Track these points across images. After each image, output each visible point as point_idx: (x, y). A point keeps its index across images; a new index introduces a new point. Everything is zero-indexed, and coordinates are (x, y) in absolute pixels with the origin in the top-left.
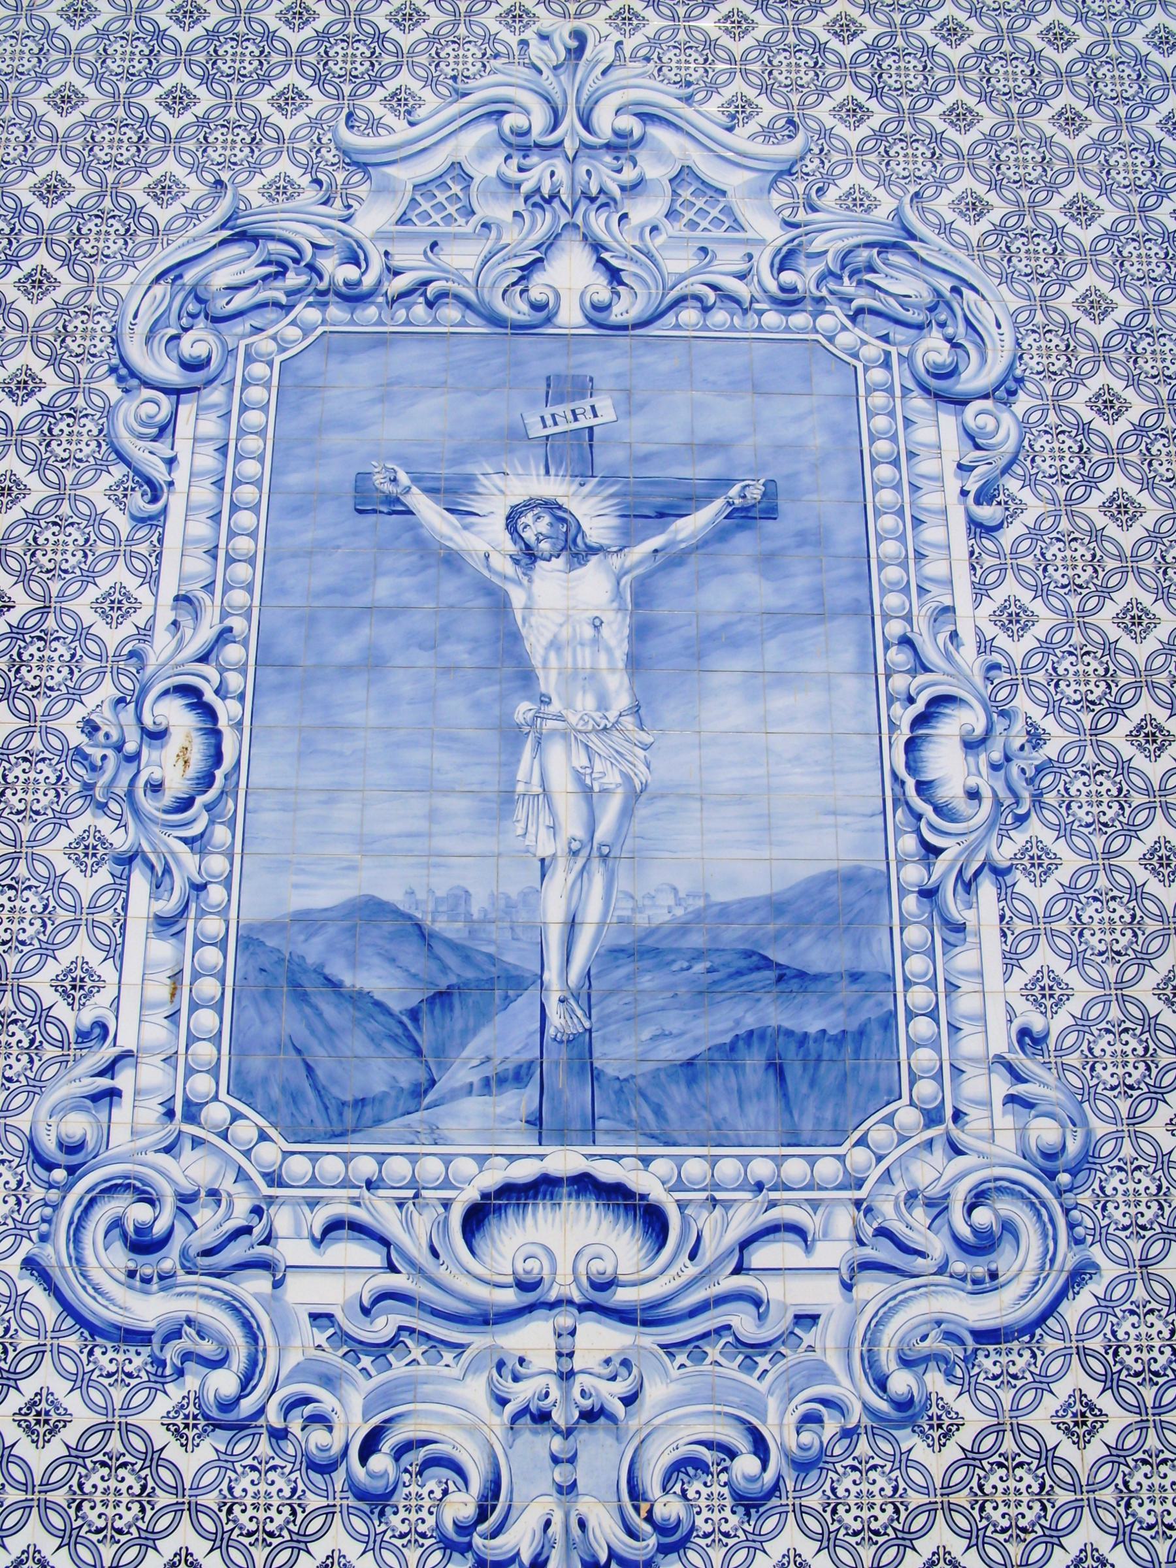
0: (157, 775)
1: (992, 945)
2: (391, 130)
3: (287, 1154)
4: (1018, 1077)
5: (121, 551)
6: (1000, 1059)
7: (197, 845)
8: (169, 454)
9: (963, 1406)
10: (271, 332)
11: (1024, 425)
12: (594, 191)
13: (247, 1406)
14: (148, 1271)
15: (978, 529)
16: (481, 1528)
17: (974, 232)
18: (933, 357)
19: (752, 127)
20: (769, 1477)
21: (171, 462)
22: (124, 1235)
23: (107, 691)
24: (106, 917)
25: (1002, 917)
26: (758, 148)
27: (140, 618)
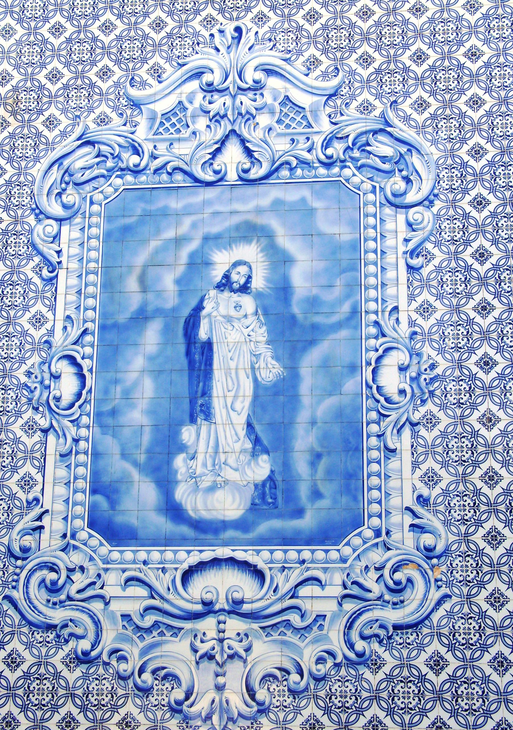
0: (58, 395)
1: (407, 458)
2: (151, 86)
3: (110, 551)
4: (415, 515)
5: (40, 296)
6: (408, 509)
7: (76, 423)
8: (59, 249)
9: (386, 656)
10: (100, 190)
11: (437, 217)
12: (243, 112)
13: (93, 654)
14: (55, 600)
15: (410, 268)
16: (186, 703)
17: (420, 118)
18: (397, 187)
19: (318, 72)
20: (303, 684)
21: (59, 252)
22: (46, 587)
23: (36, 359)
24: (38, 455)
25: (412, 446)
26: (319, 84)
27: (49, 326)
